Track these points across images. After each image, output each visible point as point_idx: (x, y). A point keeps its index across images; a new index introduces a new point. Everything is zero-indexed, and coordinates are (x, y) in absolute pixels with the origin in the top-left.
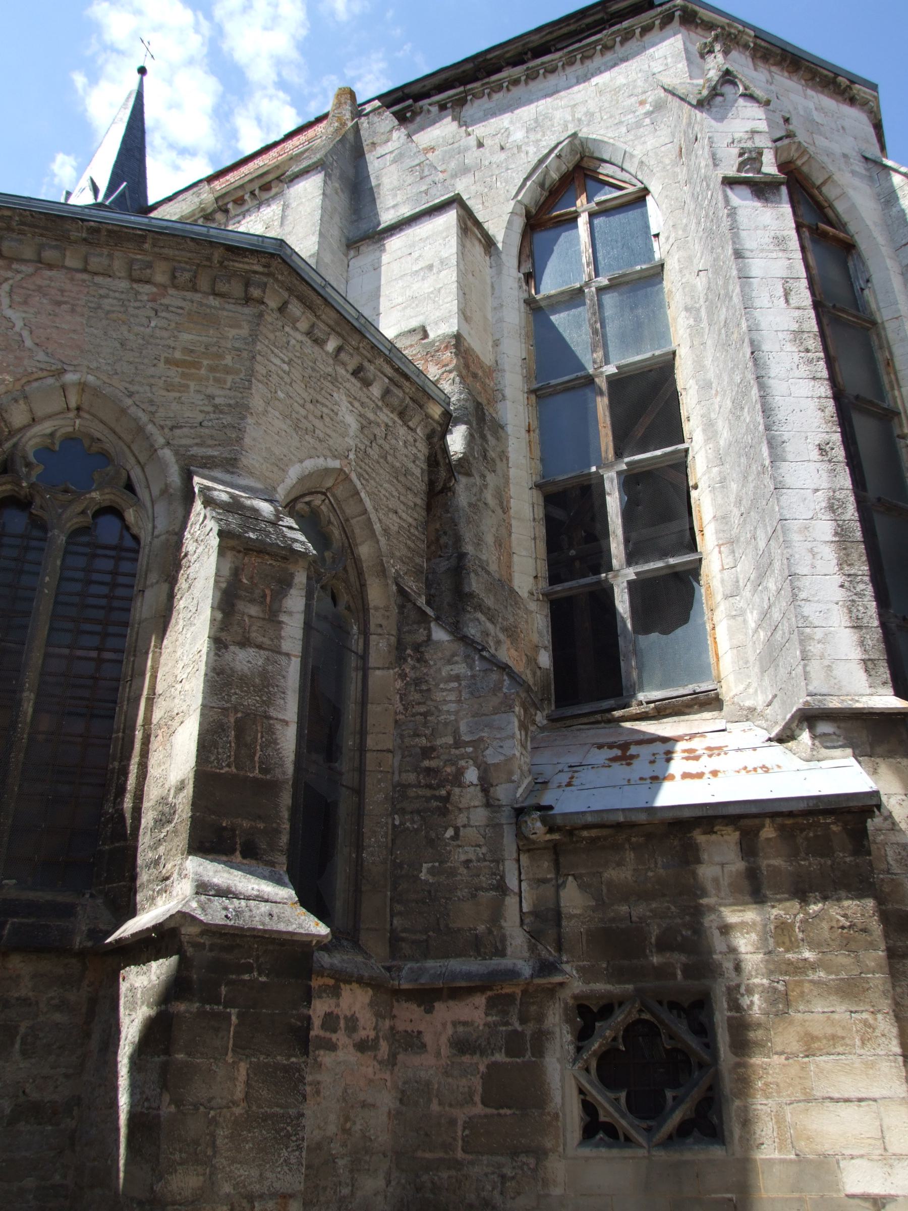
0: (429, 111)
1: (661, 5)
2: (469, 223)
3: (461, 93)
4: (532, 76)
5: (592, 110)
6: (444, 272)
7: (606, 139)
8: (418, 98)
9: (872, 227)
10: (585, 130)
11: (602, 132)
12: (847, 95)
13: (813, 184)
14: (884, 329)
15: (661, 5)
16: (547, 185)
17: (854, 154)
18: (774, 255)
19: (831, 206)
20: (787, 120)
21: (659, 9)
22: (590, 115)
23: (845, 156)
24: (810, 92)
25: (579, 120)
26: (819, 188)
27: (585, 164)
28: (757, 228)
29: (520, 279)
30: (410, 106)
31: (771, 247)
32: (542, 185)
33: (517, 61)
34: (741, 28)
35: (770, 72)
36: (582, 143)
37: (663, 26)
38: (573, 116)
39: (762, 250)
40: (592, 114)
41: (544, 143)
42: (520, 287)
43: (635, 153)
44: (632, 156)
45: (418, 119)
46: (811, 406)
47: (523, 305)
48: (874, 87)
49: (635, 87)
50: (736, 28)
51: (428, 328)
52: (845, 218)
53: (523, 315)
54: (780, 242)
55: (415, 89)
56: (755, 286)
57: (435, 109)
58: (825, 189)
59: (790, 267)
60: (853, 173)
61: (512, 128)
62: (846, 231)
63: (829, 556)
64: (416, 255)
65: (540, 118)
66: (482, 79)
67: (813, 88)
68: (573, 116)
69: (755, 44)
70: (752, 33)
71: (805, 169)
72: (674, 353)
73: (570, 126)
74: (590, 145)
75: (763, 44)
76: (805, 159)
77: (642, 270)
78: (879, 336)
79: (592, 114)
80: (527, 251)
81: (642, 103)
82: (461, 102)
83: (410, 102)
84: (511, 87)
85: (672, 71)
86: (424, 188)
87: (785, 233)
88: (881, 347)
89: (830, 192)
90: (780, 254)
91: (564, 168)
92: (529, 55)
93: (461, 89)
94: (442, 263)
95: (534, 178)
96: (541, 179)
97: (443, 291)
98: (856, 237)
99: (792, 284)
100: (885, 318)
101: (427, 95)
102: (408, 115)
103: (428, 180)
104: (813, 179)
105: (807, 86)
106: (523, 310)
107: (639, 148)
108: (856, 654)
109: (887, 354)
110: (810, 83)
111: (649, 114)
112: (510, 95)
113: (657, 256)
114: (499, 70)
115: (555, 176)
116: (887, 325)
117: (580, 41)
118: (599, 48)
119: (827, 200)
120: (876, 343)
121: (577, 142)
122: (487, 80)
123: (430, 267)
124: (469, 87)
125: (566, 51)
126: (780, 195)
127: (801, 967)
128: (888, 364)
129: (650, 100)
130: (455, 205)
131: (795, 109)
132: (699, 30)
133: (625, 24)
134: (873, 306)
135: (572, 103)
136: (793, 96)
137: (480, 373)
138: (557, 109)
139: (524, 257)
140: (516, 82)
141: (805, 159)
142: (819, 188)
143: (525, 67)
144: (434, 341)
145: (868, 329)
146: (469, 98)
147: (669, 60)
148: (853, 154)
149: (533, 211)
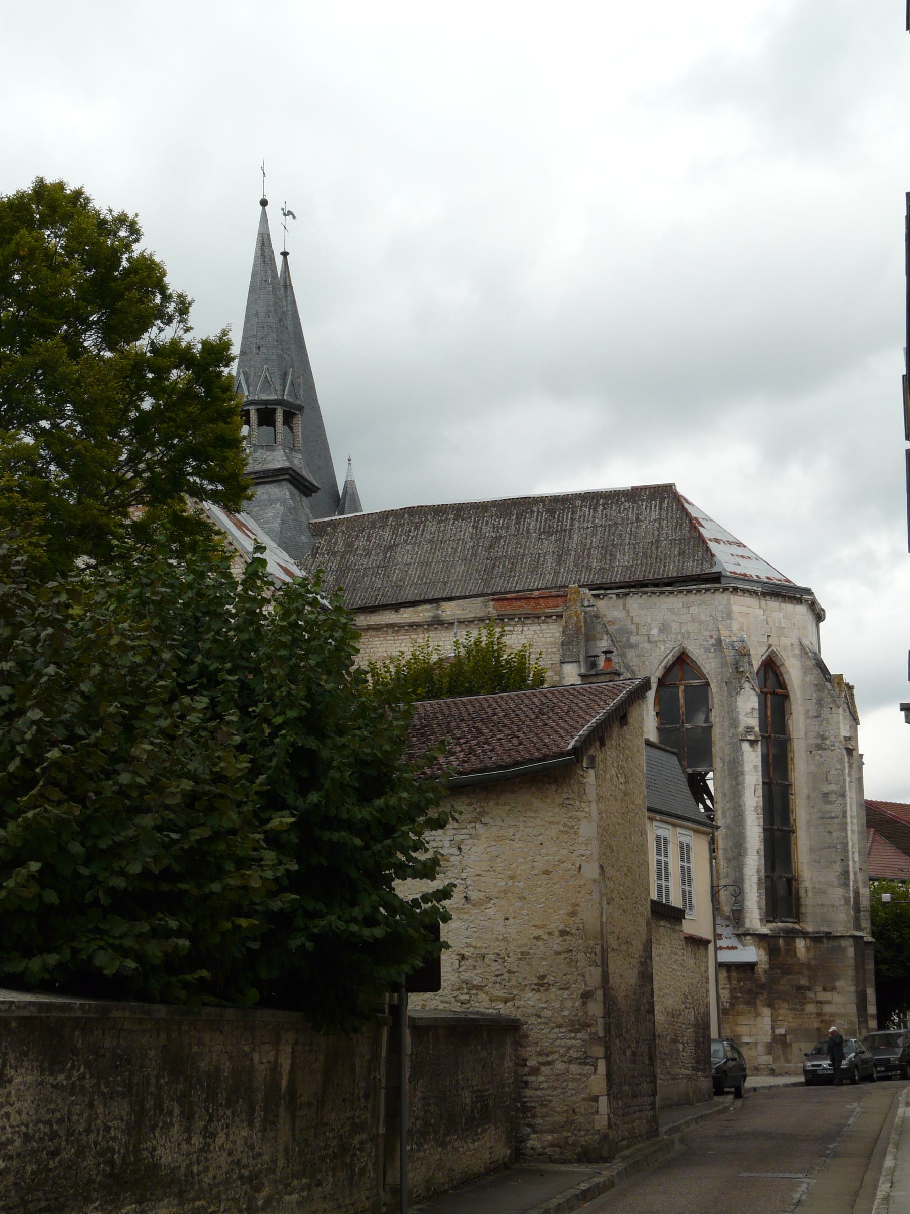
24: (783, 605)
27: (684, 657)
33: (656, 585)
46: (757, 835)
52: (787, 682)
54: (756, 767)
57: (614, 596)
60: (794, 655)
63: (755, 887)
67: (785, 602)
81: (711, 637)
82: (627, 594)
101: (611, 589)
108: (758, 917)
127: (738, 997)
133: (708, 586)
148: (796, 642)
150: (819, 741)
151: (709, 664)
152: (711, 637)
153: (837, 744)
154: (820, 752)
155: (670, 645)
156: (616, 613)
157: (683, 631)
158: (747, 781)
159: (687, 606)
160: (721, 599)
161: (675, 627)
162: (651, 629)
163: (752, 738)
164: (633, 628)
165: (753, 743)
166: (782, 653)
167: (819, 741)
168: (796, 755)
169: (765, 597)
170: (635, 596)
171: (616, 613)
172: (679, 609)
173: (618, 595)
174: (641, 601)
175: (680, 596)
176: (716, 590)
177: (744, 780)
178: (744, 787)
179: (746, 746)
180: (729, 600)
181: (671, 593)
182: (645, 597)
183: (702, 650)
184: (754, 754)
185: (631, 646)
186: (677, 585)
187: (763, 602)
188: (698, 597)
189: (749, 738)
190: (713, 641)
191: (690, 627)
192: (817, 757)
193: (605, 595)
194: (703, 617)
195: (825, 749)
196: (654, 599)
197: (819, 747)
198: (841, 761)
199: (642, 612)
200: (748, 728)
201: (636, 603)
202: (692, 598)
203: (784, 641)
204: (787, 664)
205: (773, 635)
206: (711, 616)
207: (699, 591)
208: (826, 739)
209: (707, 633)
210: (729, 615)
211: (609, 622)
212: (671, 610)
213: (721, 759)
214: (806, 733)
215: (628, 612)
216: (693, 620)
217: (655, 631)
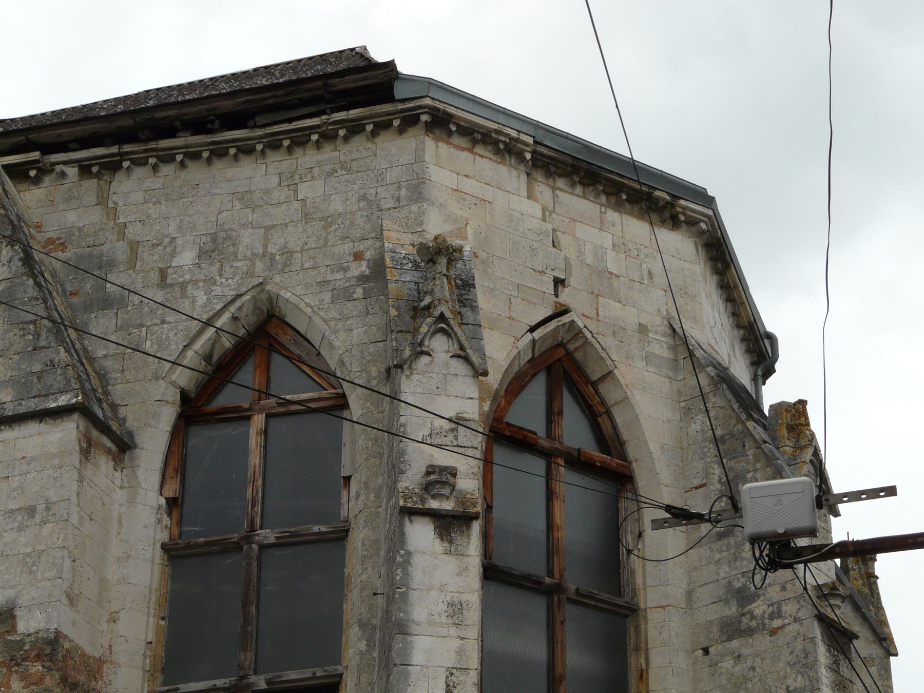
0: (63, 175)
1: (403, 101)
2: (95, 433)
3: (113, 155)
4: (219, 152)
5: (290, 246)
6: (49, 526)
7: (302, 306)
8: (48, 149)
9: (657, 454)
10: (277, 278)
11: (299, 290)
12: (667, 214)
13: (587, 381)
14: (646, 618)
15: (403, 101)
16: (215, 359)
17: (658, 321)
18: (443, 631)
19: (608, 413)
20: (559, 283)
21: (400, 106)
22: (287, 253)
23: (642, 329)
24: (612, 216)
25: (273, 257)
26: (594, 384)
27: (272, 330)
28: (430, 589)
29: (160, 507)
30: (37, 161)
31: (444, 619)
32: (208, 358)
33: (198, 126)
34: (514, 134)
35: (554, 189)
36: (270, 299)
37: (401, 131)
38: (265, 247)
39: (433, 624)
40: (291, 253)
41: (217, 290)
42: (159, 521)
43: (337, 344)
44: (331, 346)
45: (47, 180)
47: (159, 551)
48: (710, 202)
49: (352, 224)
50: (507, 135)
51: (18, 613)
52: (625, 435)
53: (157, 568)
54: (456, 609)
55: (47, 136)
56: (412, 679)
58: (603, 389)
59: (460, 652)
60: (649, 358)
61: (179, 241)
62: (623, 456)
64: (15, 482)
65: (222, 235)
66: (146, 141)
67: (618, 206)
68: (265, 247)
69: (534, 152)
70: (530, 140)
71: (578, 356)
72: (341, 676)
73: (259, 266)
74: (281, 304)
75: (545, 151)
76: (578, 343)
77: (321, 533)
78: (637, 627)
79: (291, 253)
80: (174, 461)
81: (358, 256)
82: (113, 166)
83: (35, 155)
84: (187, 162)
85: (404, 212)
86: (37, 368)
87: (464, 597)
88: (637, 649)
89: (608, 392)
90: (453, 631)
91: (242, 332)
92: (217, 124)
93: (114, 149)
94: (48, 509)
95: (197, 346)
96: (208, 348)
97: (43, 558)
98: (635, 465)
99: (459, 677)
100: (649, 605)
101: (63, 148)
102: (33, 173)
103: (45, 356)
104: (589, 372)
105: (608, 205)
106: (158, 560)
107: (342, 335)
109: (643, 661)
110: (613, 199)
111: (362, 279)
112: (183, 174)
113: (344, 513)
114: (171, 133)
115: (227, 342)
116: (651, 615)
117: (290, 121)
118: (315, 137)
119: (603, 403)
120: (633, 640)
121: (264, 296)
122: (153, 145)
123: (31, 511)
124: (127, 148)
125: (269, 130)
126: (469, 536)
128: (641, 677)
129: (368, 255)
130: (76, 416)
131: (581, 253)
132: (456, 140)
133: (354, 113)
134: (639, 580)
135: (268, 223)
136: (582, 231)
137: (82, 678)
138: (244, 226)
139: (170, 471)
140: (195, 156)
141: (578, 343)
142: (594, 384)
143: (209, 139)
144: (21, 643)
145: (626, 616)
146: (126, 164)
147: (403, 192)
148: (657, 324)
149: (193, 395)
150: (732, 610)
151: (344, 336)
152: (358, 256)
153: (789, 609)
154: (735, 644)
155: (225, 288)
156: (72, 217)
157: (272, 249)
158: (418, 657)
159: (291, 182)
160: (395, 152)
161: (248, 239)
162: (173, 254)
163: (448, 505)
164: (120, 250)
165: (449, 524)
166: (608, 342)
167: (732, 610)
168: (656, 659)
169: (549, 174)
170: (139, 172)
171: (72, 217)
172: (267, 192)
173: (85, 170)
174: (154, 182)
175: (274, 157)
176: (382, 126)
177: (407, 649)
178: (406, 676)
179: (421, 534)
180: (419, 159)
181: (246, 150)
182: (167, 169)
183: (327, 297)
184: (451, 563)
185: (106, 303)
186: (260, 120)
187: (543, 189)
188: (328, 153)
189: (434, 504)
190: (363, 268)
191: (293, 237)
192: (728, 663)
193: (44, 171)
194: (336, 205)
195: (750, 632)
196: (196, 172)
197: (732, 629)
198: (806, 664)
199: (154, 211)
200: (431, 470)
201: (133, 189)
202: (308, 158)
203: (610, 308)
204: (623, 373)
205: (573, 282)
206: (364, 198)
207: (328, 136)
208: (753, 598)
209: (348, 247)
210: (418, 190)
211: (50, 241)
212: (244, 198)
213: (362, 625)
214: (690, 594)
215: (113, 213)
216: (306, 217)
217: (186, 258)
